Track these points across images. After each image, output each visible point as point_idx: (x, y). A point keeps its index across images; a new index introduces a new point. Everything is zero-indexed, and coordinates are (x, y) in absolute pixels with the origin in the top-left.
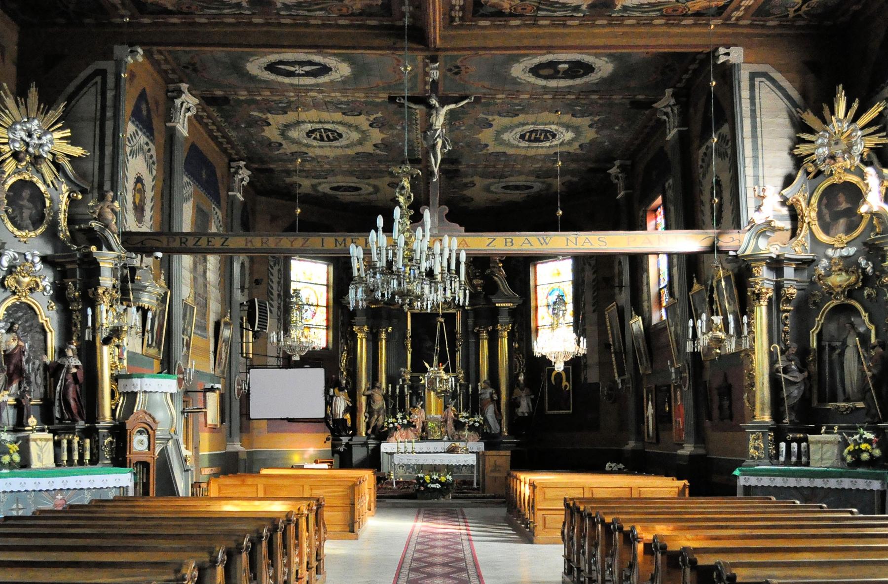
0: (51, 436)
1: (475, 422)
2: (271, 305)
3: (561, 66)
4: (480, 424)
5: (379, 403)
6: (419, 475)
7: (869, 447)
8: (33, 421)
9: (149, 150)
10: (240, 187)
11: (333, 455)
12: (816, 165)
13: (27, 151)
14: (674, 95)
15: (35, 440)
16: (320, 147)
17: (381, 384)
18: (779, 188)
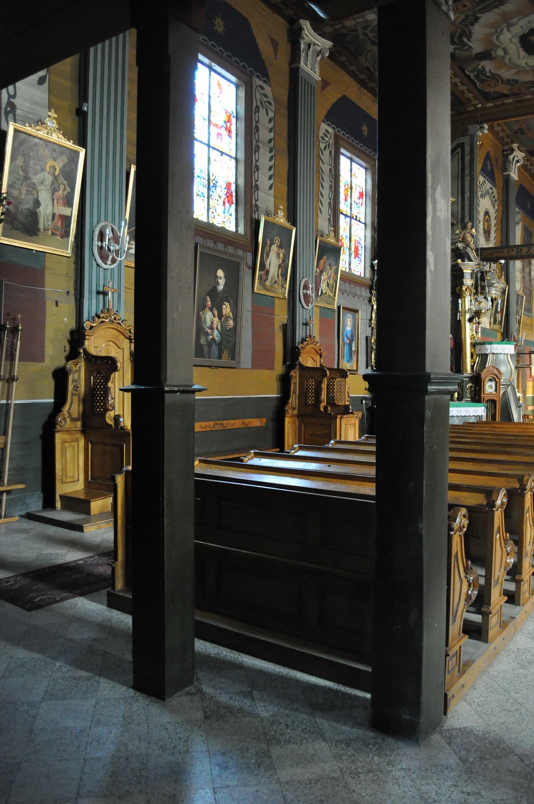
9: (493, 193)
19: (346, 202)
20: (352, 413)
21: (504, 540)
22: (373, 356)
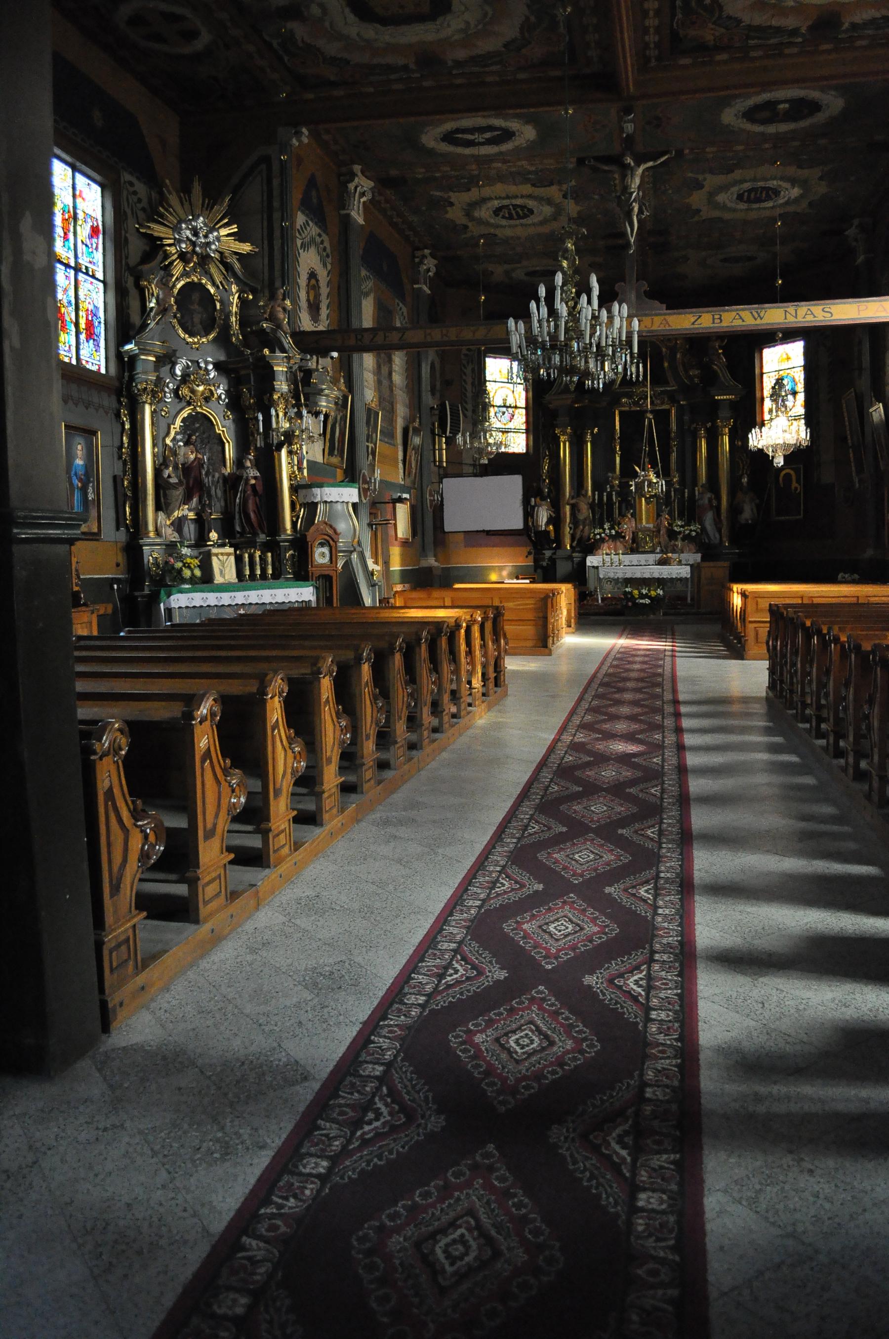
0: (232, 550)
1: (691, 531)
3: (782, 106)
4: (697, 533)
5: (585, 512)
8: (214, 535)
9: (322, 242)
11: (535, 571)
13: (194, 251)
15: (216, 555)
16: (510, 226)
17: (587, 491)
19: (66, 243)
20: (85, 605)
22: (127, 509)
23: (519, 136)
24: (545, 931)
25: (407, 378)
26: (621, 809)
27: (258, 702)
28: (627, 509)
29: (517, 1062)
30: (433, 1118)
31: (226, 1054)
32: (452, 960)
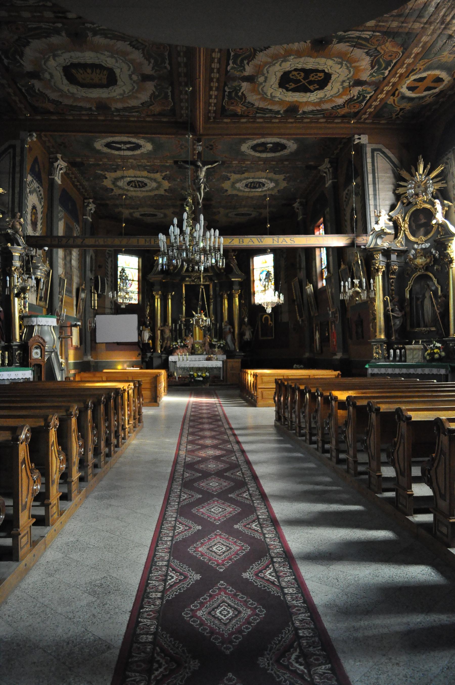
1: (221, 344)
2: (107, 280)
3: (269, 145)
5: (168, 334)
6: (191, 373)
7: (439, 351)
9: (40, 191)
10: (89, 214)
12: (408, 199)
14: (330, 162)
16: (135, 191)
17: (169, 324)
18: (388, 212)
21: (30, 469)
23: (144, 148)
24: (211, 551)
25: (79, 263)
26: (225, 484)
27: (45, 430)
28: (189, 333)
29: (225, 624)
30: (192, 663)
31: (56, 638)
32: (167, 571)
